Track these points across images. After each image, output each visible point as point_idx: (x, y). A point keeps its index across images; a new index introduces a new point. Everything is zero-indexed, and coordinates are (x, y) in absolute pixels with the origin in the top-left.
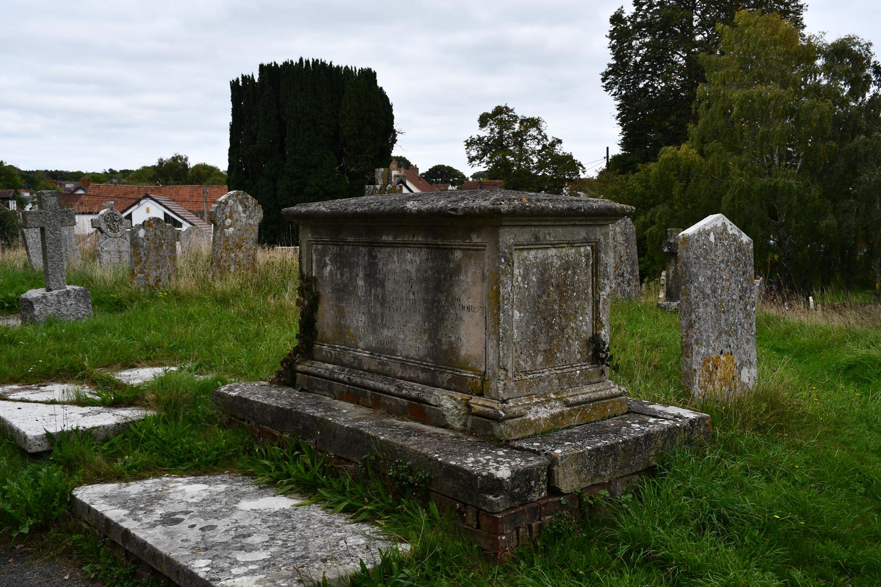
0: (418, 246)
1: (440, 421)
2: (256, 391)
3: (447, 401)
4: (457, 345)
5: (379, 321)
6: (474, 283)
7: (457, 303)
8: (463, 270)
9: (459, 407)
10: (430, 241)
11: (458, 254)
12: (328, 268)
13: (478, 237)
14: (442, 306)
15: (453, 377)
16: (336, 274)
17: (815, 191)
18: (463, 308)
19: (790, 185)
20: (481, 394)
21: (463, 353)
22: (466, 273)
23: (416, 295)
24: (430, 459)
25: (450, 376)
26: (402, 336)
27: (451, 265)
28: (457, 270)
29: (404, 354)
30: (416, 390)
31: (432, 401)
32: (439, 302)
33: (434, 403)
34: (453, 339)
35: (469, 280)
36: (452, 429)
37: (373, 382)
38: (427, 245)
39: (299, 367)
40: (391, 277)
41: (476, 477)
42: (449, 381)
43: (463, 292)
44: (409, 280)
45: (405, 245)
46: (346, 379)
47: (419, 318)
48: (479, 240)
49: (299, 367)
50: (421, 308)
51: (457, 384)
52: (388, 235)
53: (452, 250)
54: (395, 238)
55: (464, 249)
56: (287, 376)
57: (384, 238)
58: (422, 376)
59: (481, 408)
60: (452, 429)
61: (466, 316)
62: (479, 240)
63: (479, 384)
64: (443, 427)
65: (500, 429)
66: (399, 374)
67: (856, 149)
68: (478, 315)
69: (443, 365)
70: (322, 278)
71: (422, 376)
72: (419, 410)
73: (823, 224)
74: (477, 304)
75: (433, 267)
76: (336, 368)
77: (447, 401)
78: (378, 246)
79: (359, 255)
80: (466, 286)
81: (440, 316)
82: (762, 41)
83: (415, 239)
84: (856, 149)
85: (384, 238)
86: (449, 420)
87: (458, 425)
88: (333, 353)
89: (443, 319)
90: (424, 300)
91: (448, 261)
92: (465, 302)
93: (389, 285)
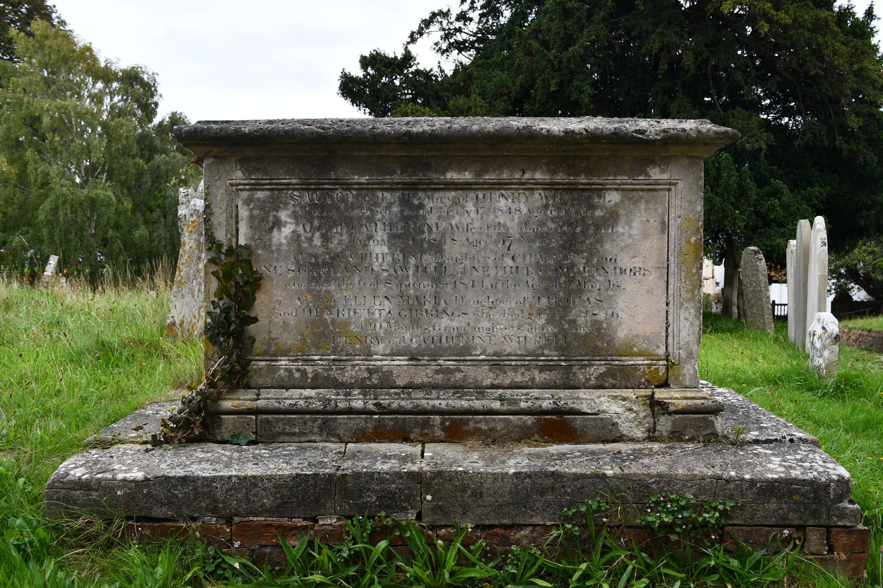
0: (528, 187)
1: (608, 433)
2: (129, 465)
3: (609, 404)
4: (609, 324)
5: (428, 306)
6: (645, 236)
7: (610, 267)
8: (623, 219)
9: (635, 408)
10: (560, 178)
11: (612, 198)
12: (287, 231)
13: (663, 172)
14: (579, 272)
15: (609, 369)
16: (310, 240)
17: (128, 204)
18: (623, 271)
19: (109, 197)
20: (665, 385)
21: (622, 334)
22: (629, 223)
23: (519, 260)
24: (728, 481)
25: (603, 369)
26: (486, 324)
27: (598, 213)
28: (612, 217)
29: (490, 350)
30: (546, 400)
31: (585, 408)
32: (572, 266)
33: (589, 411)
34: (601, 316)
35: (634, 232)
36: (632, 440)
37: (444, 403)
38: (550, 187)
39: (227, 404)
40: (460, 236)
41: (827, 486)
42: (602, 376)
43: (622, 249)
44: (505, 237)
45: (500, 185)
46: (371, 407)
47: (526, 293)
48: (665, 176)
49: (227, 404)
50: (533, 279)
51: (618, 378)
52: (461, 170)
53: (600, 191)
54: (478, 174)
55: (624, 190)
56: (198, 424)
57: (451, 176)
58: (539, 377)
59: (690, 402)
60: (632, 440)
61: (628, 283)
62: (665, 176)
63: (662, 370)
64: (614, 441)
65: (720, 424)
66: (488, 382)
67: (158, 167)
68: (653, 279)
69: (580, 352)
70: (267, 246)
71: (539, 377)
72: (558, 426)
73: (137, 234)
74: (651, 264)
75: (558, 217)
76: (329, 394)
77: (609, 404)
78: (424, 190)
79: (377, 204)
80: (629, 241)
81: (574, 286)
82: (64, 55)
83: (527, 176)
84: (158, 167)
85: (451, 176)
86: (625, 428)
87: (639, 433)
88: (309, 369)
89: (580, 291)
90: (538, 266)
91: (592, 207)
92: (625, 262)
93: (453, 250)
